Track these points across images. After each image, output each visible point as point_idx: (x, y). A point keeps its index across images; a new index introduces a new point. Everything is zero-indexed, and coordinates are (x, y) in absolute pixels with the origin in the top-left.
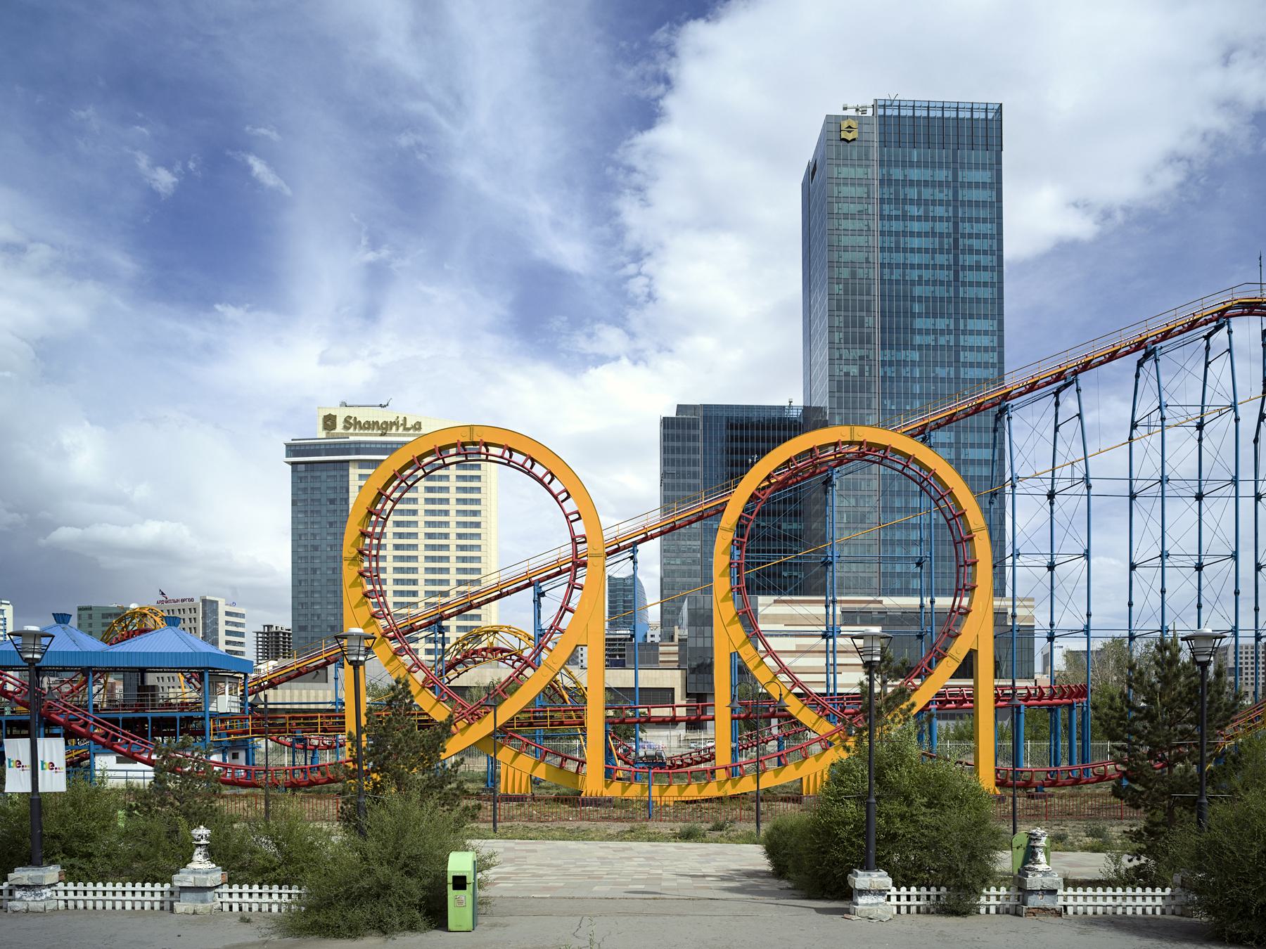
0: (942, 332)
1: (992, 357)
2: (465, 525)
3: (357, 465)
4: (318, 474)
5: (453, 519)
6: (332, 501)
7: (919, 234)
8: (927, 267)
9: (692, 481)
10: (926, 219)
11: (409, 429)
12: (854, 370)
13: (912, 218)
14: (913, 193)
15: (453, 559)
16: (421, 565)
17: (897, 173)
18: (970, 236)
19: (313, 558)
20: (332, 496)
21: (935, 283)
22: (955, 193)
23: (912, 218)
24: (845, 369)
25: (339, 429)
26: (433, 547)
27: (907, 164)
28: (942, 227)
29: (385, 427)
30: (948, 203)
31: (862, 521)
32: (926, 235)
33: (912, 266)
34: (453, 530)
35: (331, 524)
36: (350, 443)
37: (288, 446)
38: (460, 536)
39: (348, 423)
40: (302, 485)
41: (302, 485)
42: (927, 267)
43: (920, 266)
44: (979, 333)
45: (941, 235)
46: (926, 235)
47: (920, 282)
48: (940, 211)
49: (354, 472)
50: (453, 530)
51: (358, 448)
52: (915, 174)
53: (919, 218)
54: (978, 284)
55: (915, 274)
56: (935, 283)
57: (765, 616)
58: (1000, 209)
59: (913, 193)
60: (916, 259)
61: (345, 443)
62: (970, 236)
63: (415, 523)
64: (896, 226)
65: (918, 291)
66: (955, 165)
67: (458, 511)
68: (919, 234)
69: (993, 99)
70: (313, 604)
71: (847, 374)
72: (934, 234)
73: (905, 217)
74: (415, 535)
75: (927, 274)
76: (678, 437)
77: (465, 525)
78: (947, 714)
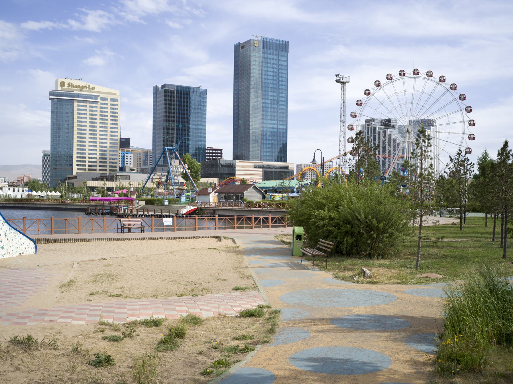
0: (275, 96)
1: (285, 103)
2: (113, 124)
3: (77, 101)
4: (62, 103)
5: (109, 122)
6: (67, 113)
7: (271, 72)
8: (272, 80)
9: (172, 111)
10: (272, 68)
11: (90, 89)
12: (256, 104)
13: (269, 67)
14: (269, 61)
15: (109, 135)
16: (98, 137)
17: (266, 56)
18: (281, 73)
19: (59, 132)
20: (67, 111)
21: (274, 84)
22: (278, 62)
23: (269, 67)
24: (254, 103)
25: (66, 87)
26: (102, 131)
27: (268, 54)
28: (276, 70)
29: (82, 88)
30: (277, 64)
31: (257, 142)
32: (272, 72)
33: (269, 79)
34: (109, 126)
35: (66, 121)
36: (75, 94)
37: (50, 92)
38: (111, 128)
39: (70, 85)
40: (56, 106)
41: (56, 106)
42: (272, 80)
43: (270, 79)
44: (283, 97)
45: (275, 72)
46: (272, 72)
47: (270, 83)
48: (275, 66)
49: (76, 104)
50: (109, 126)
51: (78, 96)
52: (270, 56)
53: (271, 68)
54: (283, 85)
55: (269, 81)
56: (274, 84)
57: (237, 165)
58: (288, 67)
59: (269, 61)
60: (270, 77)
61: (73, 94)
62: (281, 73)
63: (96, 123)
64: (266, 69)
65: (270, 86)
66: (278, 55)
67: (111, 119)
68: (271, 72)
69: (287, 40)
70: (59, 148)
71: (254, 105)
72: (274, 72)
73: (268, 67)
74: (96, 127)
75: (272, 82)
76: (168, 96)
77: (113, 124)
78: (27, 201)
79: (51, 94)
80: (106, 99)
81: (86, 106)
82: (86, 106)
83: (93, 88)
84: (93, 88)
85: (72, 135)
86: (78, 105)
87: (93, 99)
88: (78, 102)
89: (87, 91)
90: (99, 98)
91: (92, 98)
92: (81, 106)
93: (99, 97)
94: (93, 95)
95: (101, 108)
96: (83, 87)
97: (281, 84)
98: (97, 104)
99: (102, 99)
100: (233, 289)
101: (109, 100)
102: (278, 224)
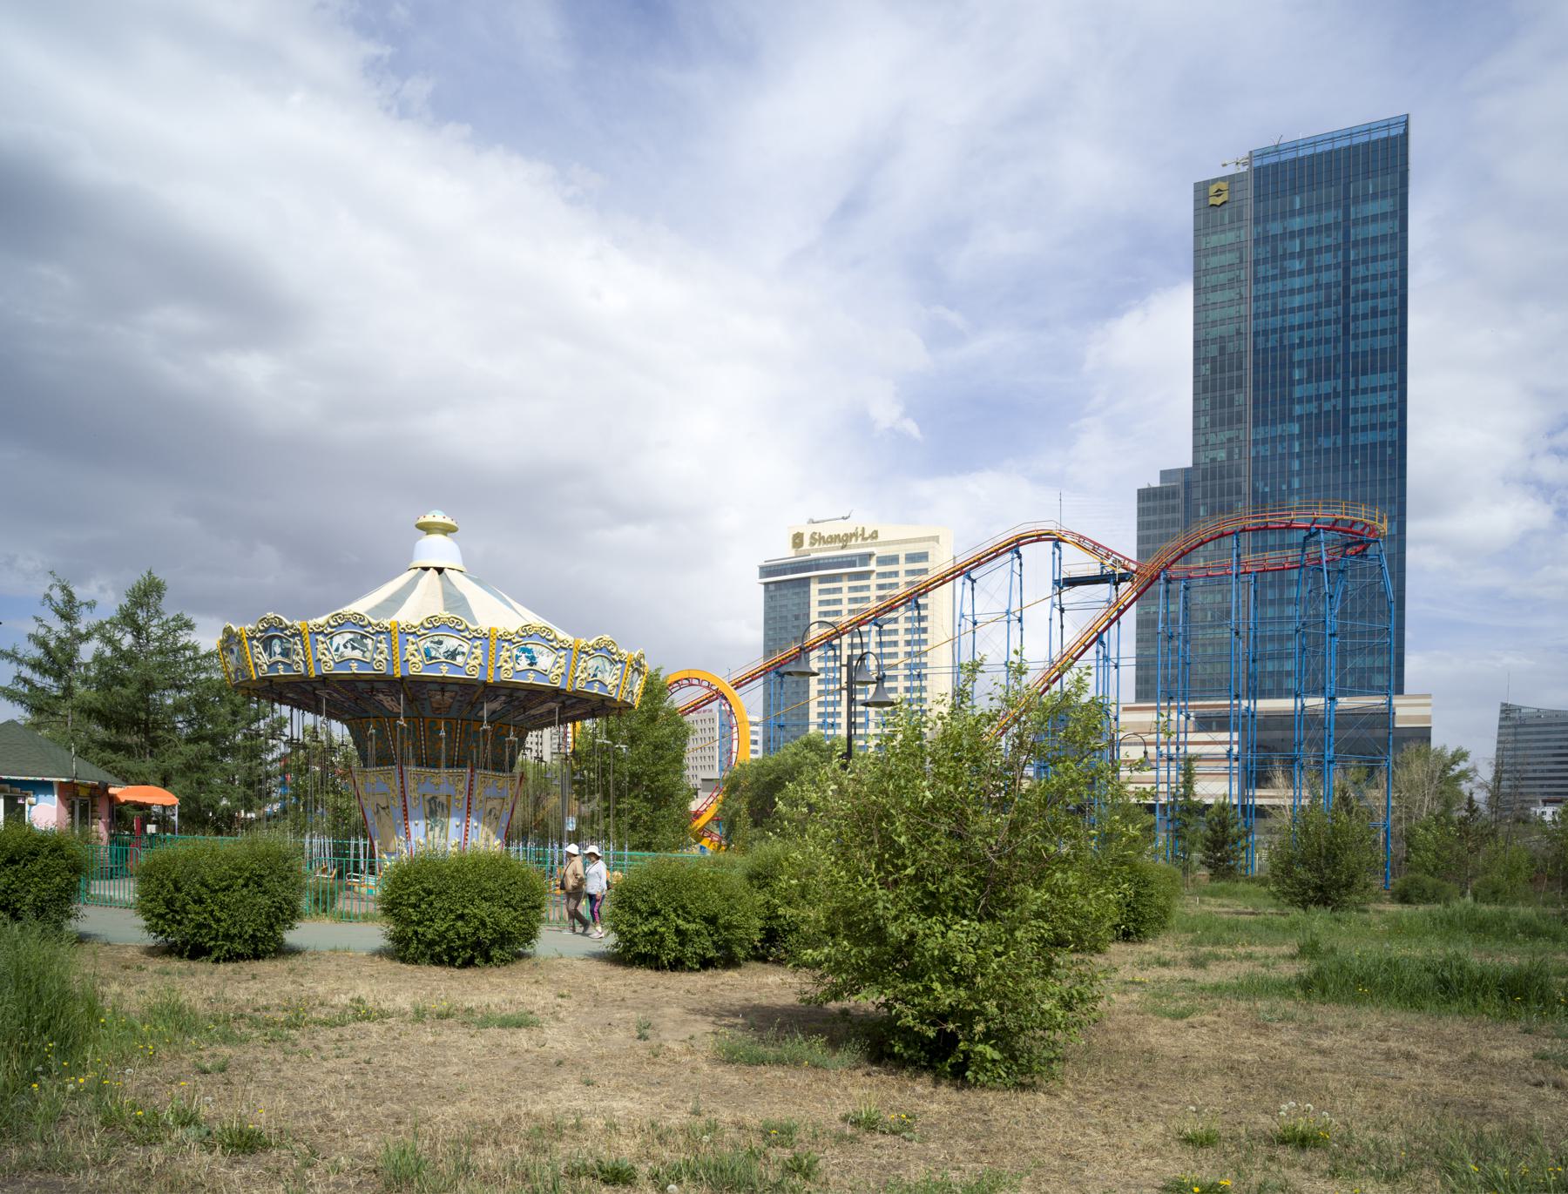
25: (806, 545)
49: (815, 588)
79: (766, 571)
80: (894, 559)
81: (839, 590)
82: (839, 590)
83: (875, 535)
84: (875, 535)
85: (456, 688)
86: (821, 591)
87: (854, 566)
88: (850, 580)
89: (858, 546)
90: (873, 561)
91: (852, 564)
92: (828, 591)
93: (874, 558)
94: (855, 555)
95: (881, 587)
96: (849, 537)
97: (1389, 223)
98: (868, 578)
99: (883, 561)
100: (374, 954)
101: (902, 560)
102: (626, 852)
